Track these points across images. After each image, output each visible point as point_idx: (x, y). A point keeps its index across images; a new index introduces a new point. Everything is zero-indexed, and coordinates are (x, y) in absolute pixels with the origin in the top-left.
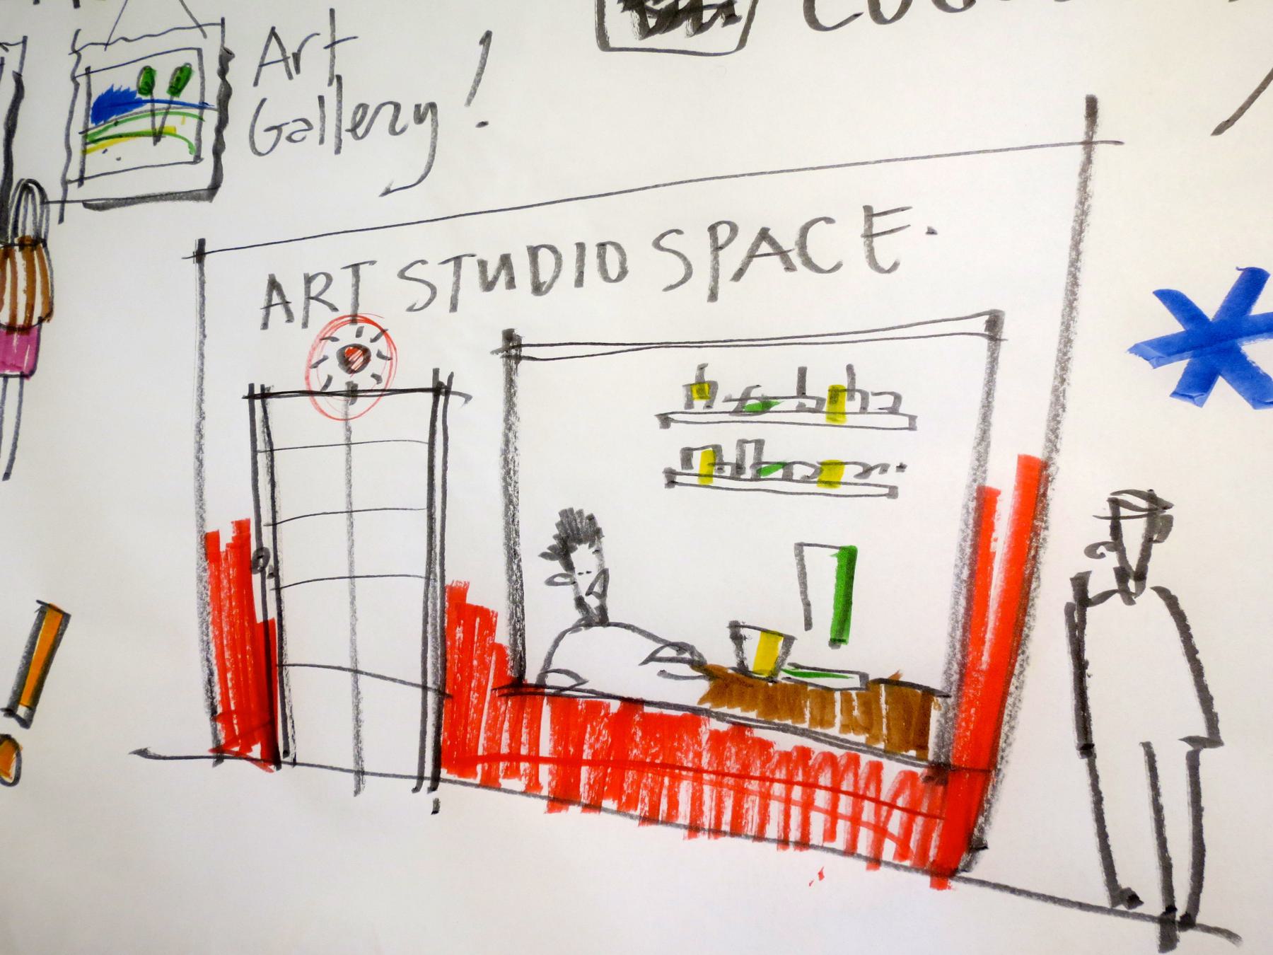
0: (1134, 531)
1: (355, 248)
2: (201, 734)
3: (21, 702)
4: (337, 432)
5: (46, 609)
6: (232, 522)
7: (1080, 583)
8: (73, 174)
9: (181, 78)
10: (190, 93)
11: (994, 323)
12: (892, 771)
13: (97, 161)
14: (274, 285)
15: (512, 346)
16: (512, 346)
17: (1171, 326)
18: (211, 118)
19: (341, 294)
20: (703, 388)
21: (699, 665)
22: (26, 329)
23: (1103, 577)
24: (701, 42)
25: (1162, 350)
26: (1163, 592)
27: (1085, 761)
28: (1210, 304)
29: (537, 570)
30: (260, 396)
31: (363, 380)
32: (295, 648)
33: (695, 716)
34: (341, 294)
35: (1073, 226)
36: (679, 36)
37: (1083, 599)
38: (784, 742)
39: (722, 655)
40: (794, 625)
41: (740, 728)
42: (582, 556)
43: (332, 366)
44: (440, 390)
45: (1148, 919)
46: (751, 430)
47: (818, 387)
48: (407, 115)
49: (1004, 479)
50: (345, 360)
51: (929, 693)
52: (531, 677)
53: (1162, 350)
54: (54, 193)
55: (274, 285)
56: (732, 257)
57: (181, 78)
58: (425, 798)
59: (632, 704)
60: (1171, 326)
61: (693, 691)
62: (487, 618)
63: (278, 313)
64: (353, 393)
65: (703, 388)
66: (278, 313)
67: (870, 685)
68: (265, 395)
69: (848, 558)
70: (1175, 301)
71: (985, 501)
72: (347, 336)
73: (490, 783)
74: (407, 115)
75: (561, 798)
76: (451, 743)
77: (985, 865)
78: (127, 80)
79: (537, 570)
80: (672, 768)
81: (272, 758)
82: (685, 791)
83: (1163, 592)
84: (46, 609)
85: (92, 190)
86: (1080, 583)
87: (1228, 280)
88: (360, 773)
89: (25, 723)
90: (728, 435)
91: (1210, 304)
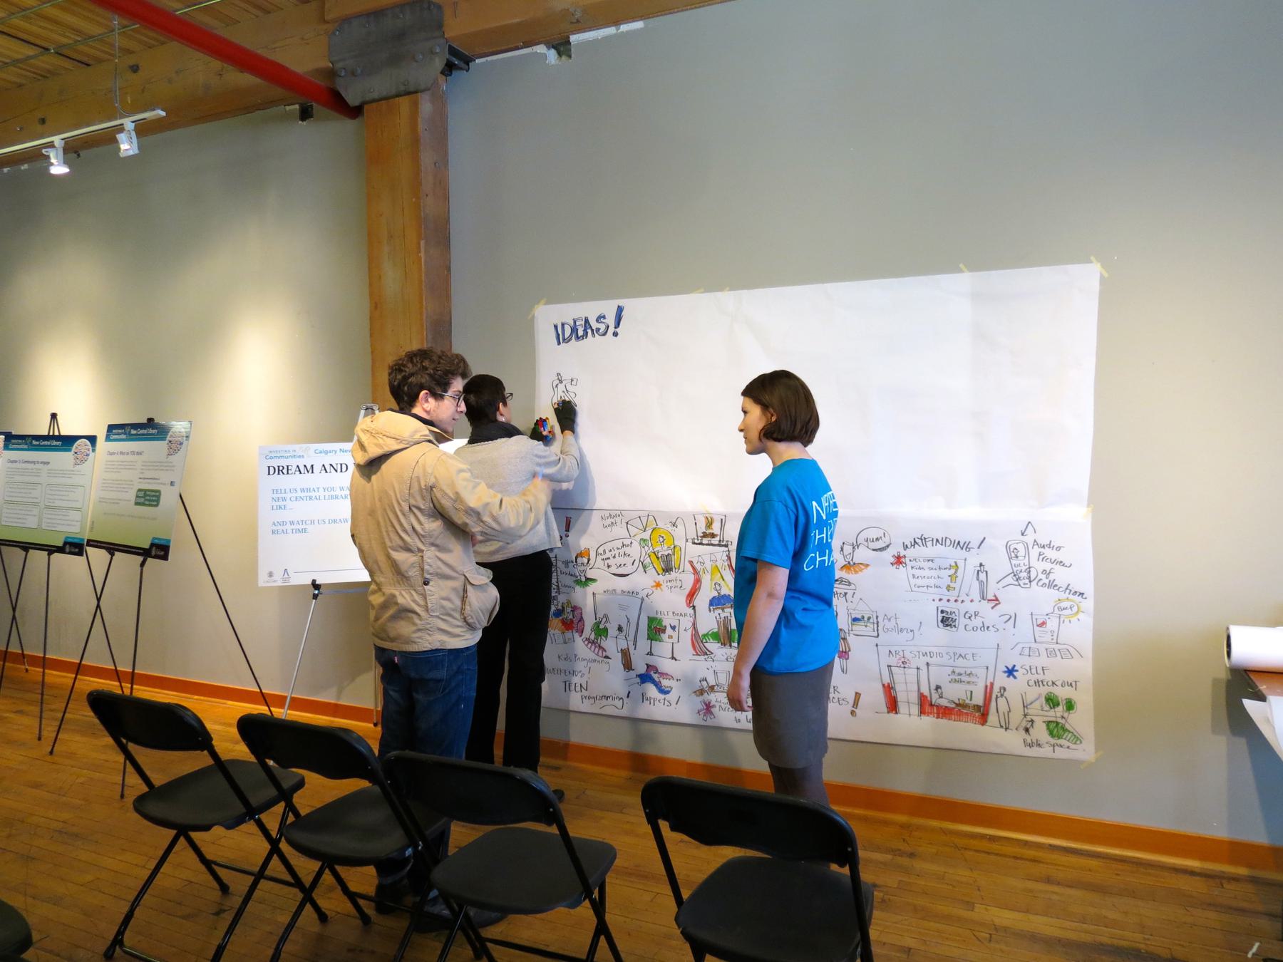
0: (1002, 691)
1: (903, 648)
2: (886, 710)
3: (751, 737)
4: (903, 672)
5: (856, 693)
6: (169, 541)
7: (997, 696)
8: (850, 629)
9: (869, 618)
10: (871, 620)
11: (987, 668)
12: (977, 714)
13: (854, 627)
14: (890, 651)
15: (928, 664)
16: (928, 664)
17: (1006, 670)
18: (876, 626)
19: (901, 653)
20: (953, 672)
21: (954, 703)
22: (845, 652)
23: (999, 695)
24: (951, 629)
25: (1005, 672)
26: (1006, 697)
27: (922, 691)
28: (1010, 668)
29: (933, 691)
30: (889, 666)
31: (906, 666)
32: (899, 699)
33: (954, 708)
34: (901, 653)
35: (561, 802)
36: (949, 628)
37: (997, 697)
38: (965, 711)
39: (957, 702)
40: (965, 699)
41: (960, 710)
42: (939, 690)
43: (901, 663)
44: (918, 668)
45: (693, 591)
46: (959, 677)
47: (968, 673)
48: (909, 631)
49: (989, 684)
50: (903, 663)
51: (981, 707)
52: (933, 703)
53: (1005, 672)
54: (847, 631)
55: (890, 651)
56: (956, 657)
57: (869, 618)
58: (919, 718)
59: (946, 707)
60: (1006, 670)
61: (953, 706)
62: (926, 697)
63: (891, 655)
64: (905, 667)
65: (953, 672)
66: (891, 655)
67: (974, 706)
68: (890, 666)
69: (971, 692)
70: (1007, 667)
71: (986, 686)
72: (903, 660)
73: (928, 716)
74: (909, 631)
75: (938, 717)
76: (776, 421)
77: (988, 724)
78: (859, 616)
79: (933, 691)
80: (952, 714)
81: (896, 713)
82: (953, 717)
83: (1006, 697)
84: (856, 693)
85: (854, 632)
86: (997, 696)
87: (1012, 666)
88: (910, 715)
89: (856, 708)
90: (957, 678)
91: (1010, 668)
